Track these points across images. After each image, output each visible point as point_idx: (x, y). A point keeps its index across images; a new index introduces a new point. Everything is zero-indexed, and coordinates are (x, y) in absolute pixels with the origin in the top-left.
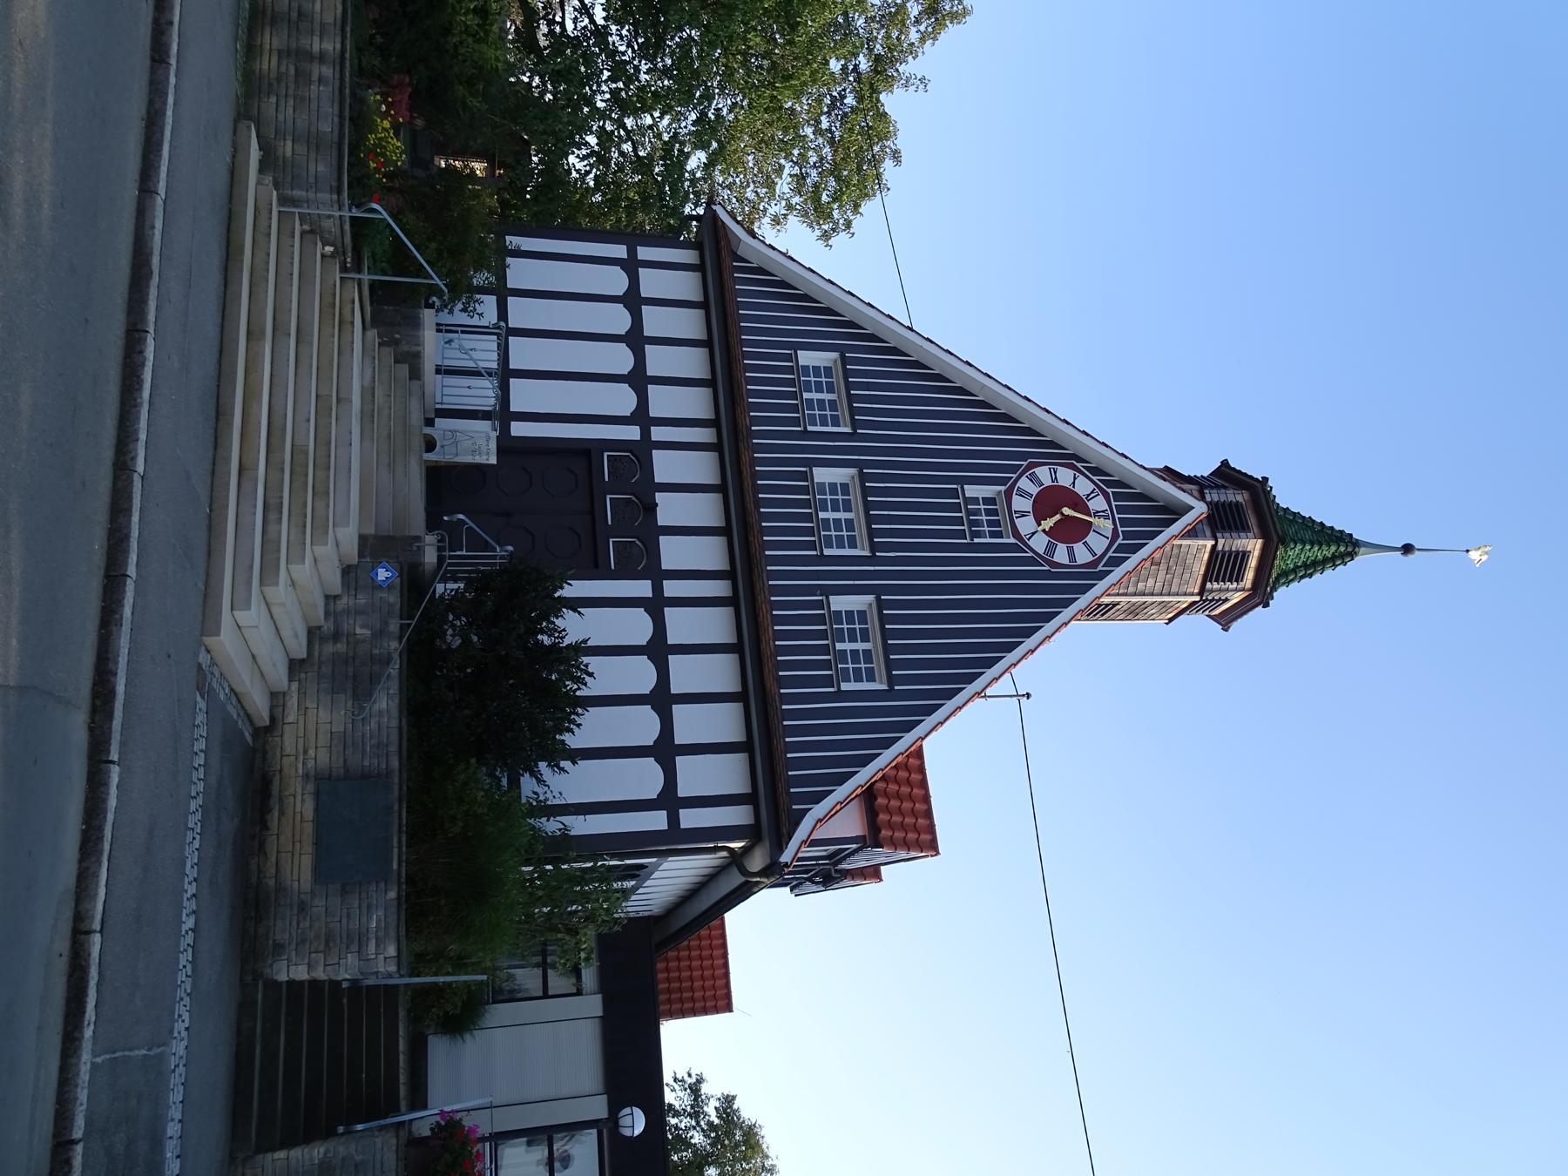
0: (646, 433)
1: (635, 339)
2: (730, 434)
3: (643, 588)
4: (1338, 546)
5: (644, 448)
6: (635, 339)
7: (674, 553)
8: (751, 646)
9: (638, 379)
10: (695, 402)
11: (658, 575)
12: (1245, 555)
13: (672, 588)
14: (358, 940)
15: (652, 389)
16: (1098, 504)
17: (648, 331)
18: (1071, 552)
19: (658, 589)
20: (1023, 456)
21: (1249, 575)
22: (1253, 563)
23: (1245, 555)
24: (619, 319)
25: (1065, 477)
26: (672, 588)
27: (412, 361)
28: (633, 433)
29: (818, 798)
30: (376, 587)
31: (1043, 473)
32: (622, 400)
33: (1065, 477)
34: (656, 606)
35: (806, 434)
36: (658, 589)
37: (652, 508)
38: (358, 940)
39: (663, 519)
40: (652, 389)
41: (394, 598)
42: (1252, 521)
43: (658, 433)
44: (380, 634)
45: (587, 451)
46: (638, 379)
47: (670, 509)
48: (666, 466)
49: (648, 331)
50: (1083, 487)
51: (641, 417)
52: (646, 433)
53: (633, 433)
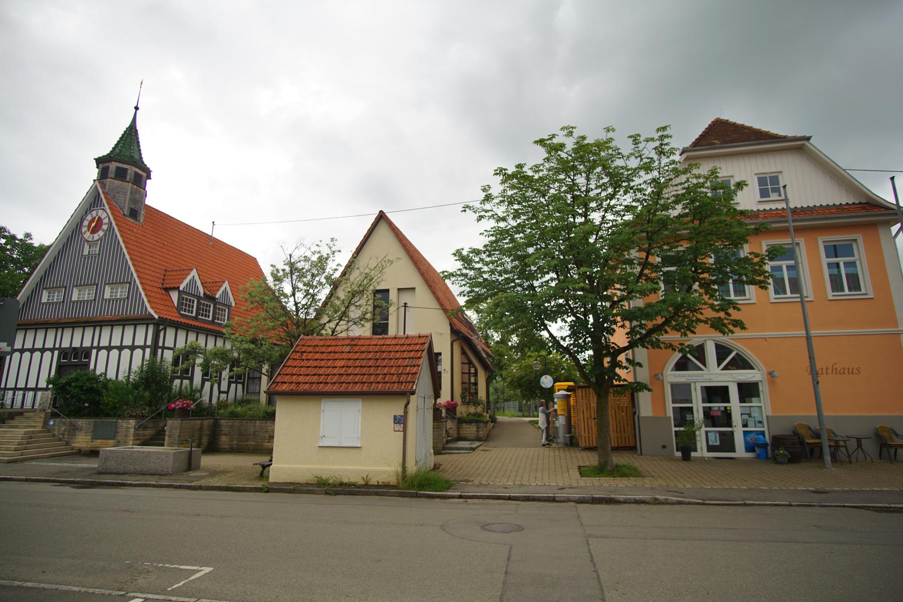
0: (57, 349)
1: (121, 348)
2: (60, 325)
4: (131, 136)
5: (60, 349)
6: (121, 348)
7: (87, 343)
8: (112, 323)
9: (132, 348)
10: (51, 334)
11: (92, 347)
12: (118, 168)
13: (95, 344)
14: (128, 428)
15: (136, 344)
16: (94, 213)
17: (130, 344)
19: (95, 348)
21: (125, 166)
22: (121, 165)
23: (118, 168)
24: (37, 355)
25: (86, 223)
26: (95, 344)
27: (20, 413)
28: (56, 353)
29: (146, 309)
30: (54, 424)
31: (84, 229)
32: (48, 355)
33: (86, 223)
34: (99, 348)
35: (128, 298)
36: (95, 348)
37: (75, 349)
38: (128, 428)
39: (78, 345)
40: (136, 344)
41: (58, 420)
42: (107, 165)
43: (57, 346)
44: (64, 424)
46: (132, 348)
47: (76, 344)
48: (66, 344)
49: (130, 344)
50: (89, 218)
51: (52, 350)
52: (57, 349)
53: (56, 353)
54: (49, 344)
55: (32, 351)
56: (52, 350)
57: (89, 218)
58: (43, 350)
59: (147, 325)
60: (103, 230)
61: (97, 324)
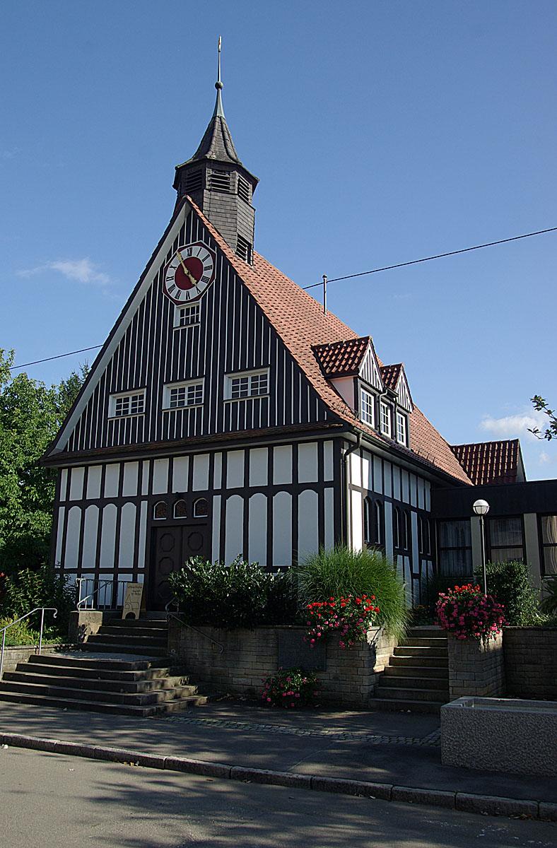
0: (145, 498)
2: (145, 452)
3: (217, 500)
5: (151, 498)
7: (201, 485)
11: (211, 492)
18: (207, 268)
19: (217, 492)
20: (161, 295)
28: (144, 504)
32: (129, 508)
33: (171, 272)
34: (226, 493)
36: (217, 492)
37: (179, 495)
43: (145, 492)
45: (153, 530)
47: (180, 486)
48: (160, 488)
51: (136, 500)
52: (145, 498)
53: (144, 504)
54: (130, 490)
55: (101, 503)
56: (136, 500)
57: (175, 263)
58: (120, 501)
59: (212, 454)
60: (205, 279)
61: (217, 444)
